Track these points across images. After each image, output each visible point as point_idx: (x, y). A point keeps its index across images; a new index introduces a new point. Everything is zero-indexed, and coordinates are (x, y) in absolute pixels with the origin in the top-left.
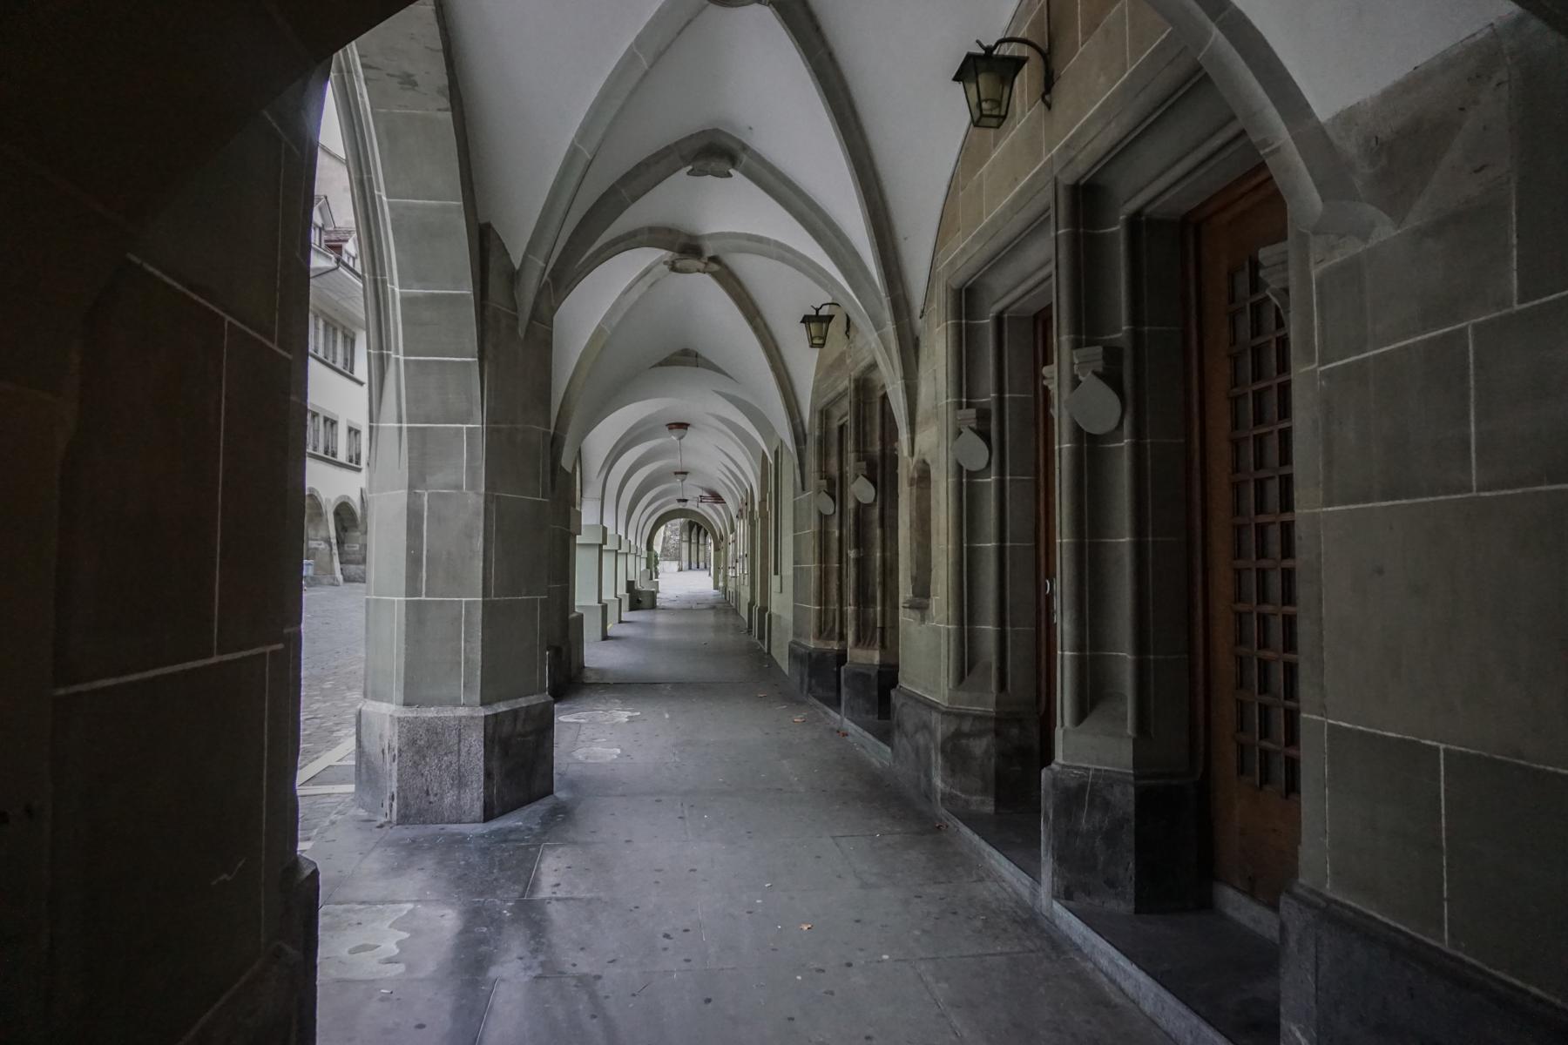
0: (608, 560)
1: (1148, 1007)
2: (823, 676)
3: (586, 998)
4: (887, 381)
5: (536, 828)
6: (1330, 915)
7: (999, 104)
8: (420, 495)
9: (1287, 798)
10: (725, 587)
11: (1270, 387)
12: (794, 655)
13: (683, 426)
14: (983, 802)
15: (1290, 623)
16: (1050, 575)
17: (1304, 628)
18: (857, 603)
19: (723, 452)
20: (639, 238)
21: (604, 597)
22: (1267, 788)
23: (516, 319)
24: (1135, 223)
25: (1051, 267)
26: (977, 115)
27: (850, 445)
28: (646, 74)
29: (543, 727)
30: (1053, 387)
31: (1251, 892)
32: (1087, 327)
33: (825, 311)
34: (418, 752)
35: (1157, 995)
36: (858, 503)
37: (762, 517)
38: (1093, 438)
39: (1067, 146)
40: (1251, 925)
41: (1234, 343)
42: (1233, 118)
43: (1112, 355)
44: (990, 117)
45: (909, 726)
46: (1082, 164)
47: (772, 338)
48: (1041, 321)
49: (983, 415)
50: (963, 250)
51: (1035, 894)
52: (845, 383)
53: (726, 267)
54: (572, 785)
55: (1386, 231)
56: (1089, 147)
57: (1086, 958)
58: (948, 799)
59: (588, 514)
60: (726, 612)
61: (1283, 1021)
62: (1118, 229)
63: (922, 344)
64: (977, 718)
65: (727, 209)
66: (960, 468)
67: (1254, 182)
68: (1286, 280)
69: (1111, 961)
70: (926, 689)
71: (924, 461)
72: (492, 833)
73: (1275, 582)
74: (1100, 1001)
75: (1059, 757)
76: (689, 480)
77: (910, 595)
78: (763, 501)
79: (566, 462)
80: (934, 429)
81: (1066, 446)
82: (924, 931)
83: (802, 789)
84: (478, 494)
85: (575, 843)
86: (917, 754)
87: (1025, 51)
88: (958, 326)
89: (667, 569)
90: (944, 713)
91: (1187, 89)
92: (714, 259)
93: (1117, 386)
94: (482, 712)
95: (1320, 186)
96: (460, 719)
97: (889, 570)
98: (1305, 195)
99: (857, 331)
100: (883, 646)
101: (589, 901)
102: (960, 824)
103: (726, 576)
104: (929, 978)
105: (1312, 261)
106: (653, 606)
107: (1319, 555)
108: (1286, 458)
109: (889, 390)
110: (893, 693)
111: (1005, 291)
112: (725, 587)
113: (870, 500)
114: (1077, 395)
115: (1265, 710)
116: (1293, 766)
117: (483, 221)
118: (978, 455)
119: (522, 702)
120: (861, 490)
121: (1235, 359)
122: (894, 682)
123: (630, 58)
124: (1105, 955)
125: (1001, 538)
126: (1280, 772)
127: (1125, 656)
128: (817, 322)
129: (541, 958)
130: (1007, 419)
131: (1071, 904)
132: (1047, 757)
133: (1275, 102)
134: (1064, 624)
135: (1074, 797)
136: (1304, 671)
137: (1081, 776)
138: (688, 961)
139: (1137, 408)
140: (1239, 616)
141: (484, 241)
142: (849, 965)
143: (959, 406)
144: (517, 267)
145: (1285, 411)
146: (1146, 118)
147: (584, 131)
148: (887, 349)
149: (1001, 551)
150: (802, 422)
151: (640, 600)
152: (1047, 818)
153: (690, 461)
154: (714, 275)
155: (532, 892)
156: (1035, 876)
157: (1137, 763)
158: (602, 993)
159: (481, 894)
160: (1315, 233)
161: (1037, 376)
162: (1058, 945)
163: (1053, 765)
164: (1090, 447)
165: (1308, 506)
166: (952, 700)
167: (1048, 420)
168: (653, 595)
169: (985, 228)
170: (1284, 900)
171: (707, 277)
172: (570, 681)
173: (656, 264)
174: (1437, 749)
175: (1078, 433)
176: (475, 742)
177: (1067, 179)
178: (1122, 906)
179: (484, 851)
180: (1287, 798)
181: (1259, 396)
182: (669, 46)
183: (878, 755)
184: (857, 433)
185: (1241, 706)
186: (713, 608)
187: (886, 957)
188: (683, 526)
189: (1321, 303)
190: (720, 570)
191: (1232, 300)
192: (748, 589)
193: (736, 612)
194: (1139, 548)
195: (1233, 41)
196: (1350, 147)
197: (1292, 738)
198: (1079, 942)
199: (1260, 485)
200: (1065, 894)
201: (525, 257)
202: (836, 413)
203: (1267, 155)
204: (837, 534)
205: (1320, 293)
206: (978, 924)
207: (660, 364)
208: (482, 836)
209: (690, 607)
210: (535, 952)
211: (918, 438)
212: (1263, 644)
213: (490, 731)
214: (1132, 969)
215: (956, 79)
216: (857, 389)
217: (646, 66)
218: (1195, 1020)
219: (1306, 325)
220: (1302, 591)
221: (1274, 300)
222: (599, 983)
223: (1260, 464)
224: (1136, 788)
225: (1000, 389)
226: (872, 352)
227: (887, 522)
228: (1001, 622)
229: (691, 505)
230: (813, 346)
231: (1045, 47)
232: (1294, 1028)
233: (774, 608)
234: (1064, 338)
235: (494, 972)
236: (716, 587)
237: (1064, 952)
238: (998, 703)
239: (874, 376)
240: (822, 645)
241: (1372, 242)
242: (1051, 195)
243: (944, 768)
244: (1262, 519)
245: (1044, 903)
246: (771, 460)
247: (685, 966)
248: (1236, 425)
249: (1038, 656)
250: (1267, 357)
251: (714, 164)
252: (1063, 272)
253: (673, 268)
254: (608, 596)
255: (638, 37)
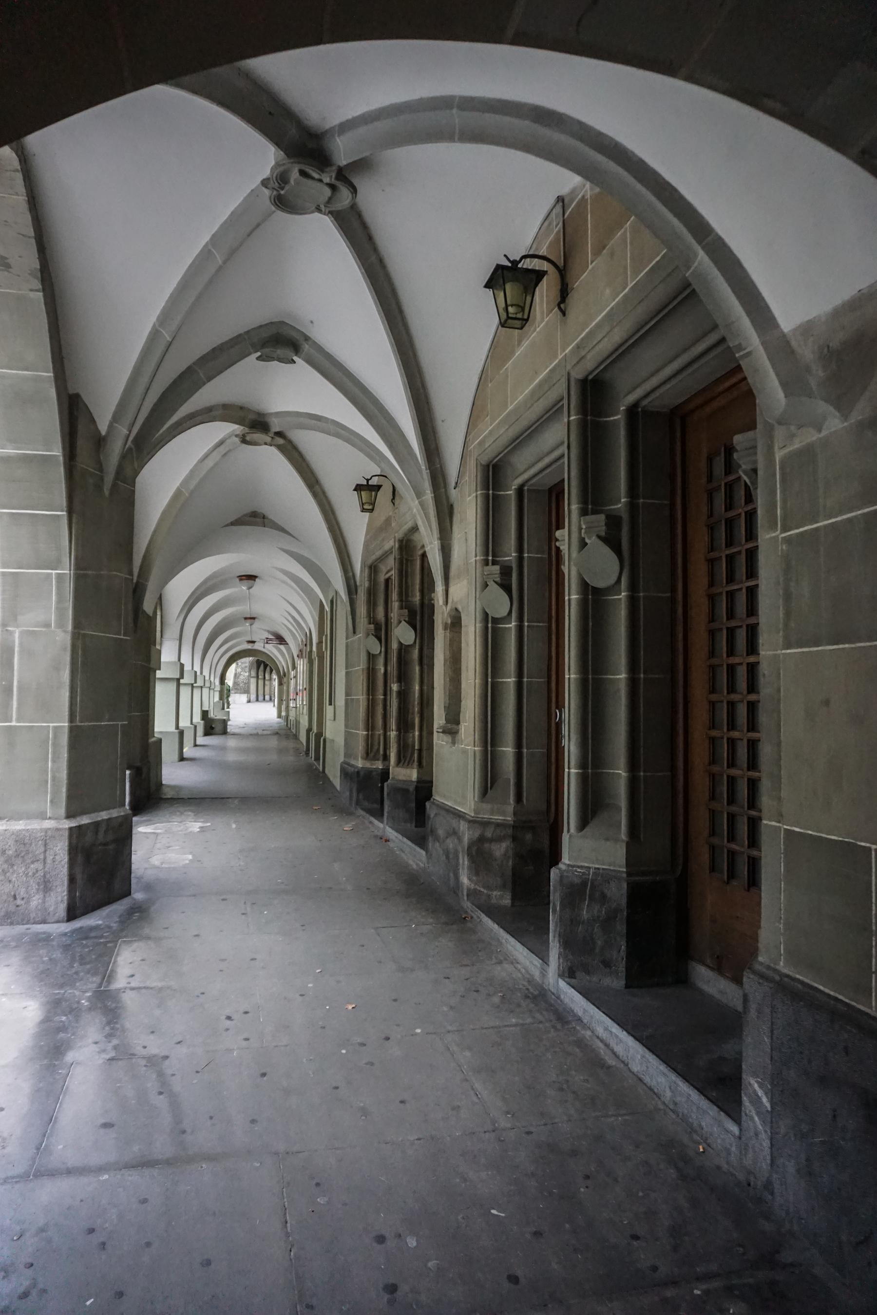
0: (185, 692)
1: (636, 1068)
2: (368, 790)
3: (154, 1076)
4: (426, 541)
5: (115, 926)
6: (784, 988)
7: (523, 309)
8: (11, 633)
9: (748, 890)
10: (287, 717)
11: (739, 552)
12: (346, 774)
13: (252, 578)
14: (502, 897)
15: (753, 745)
16: (560, 705)
17: (766, 751)
18: (399, 729)
19: (285, 601)
20: (214, 413)
21: (181, 724)
22: (734, 883)
23: (102, 479)
24: (632, 412)
25: (564, 449)
26: (504, 316)
27: (395, 596)
28: (220, 268)
29: (121, 837)
30: (564, 548)
31: (719, 968)
32: (593, 498)
33: (374, 481)
34: (6, 861)
35: (643, 1057)
36: (400, 644)
37: (319, 658)
38: (596, 591)
39: (578, 347)
40: (718, 996)
41: (711, 515)
42: (715, 327)
43: (613, 522)
44: (515, 319)
45: (441, 832)
46: (589, 364)
47: (329, 503)
48: (556, 493)
49: (506, 571)
50: (491, 432)
51: (544, 973)
52: (390, 543)
53: (290, 442)
54: (148, 887)
55: (835, 424)
56: (597, 348)
57: (586, 1027)
58: (472, 894)
59: (167, 654)
60: (287, 737)
61: (744, 1076)
62: (618, 417)
63: (455, 511)
64: (498, 825)
65: (291, 391)
66: (486, 615)
67: (727, 384)
68: (755, 462)
69: (606, 1029)
70: (455, 802)
71: (456, 609)
72: (74, 931)
73: (742, 711)
74: (594, 1062)
75: (566, 859)
76: (257, 625)
77: (443, 722)
78: (320, 643)
79: (148, 606)
80: (465, 582)
81: (574, 597)
82: (451, 1007)
83: (349, 888)
84: (65, 632)
85: (149, 938)
86: (447, 857)
87: (545, 266)
88: (486, 497)
89: (238, 700)
90: (470, 822)
91: (677, 301)
92: (279, 434)
93: (616, 548)
94: (67, 824)
95: (784, 385)
96: (46, 830)
97: (426, 702)
98: (772, 392)
99: (401, 497)
100: (420, 765)
101: (161, 989)
102: (483, 916)
103: (287, 707)
104: (455, 1048)
105: (776, 448)
106: (224, 732)
107: (779, 690)
108: (752, 610)
109: (427, 549)
110: (428, 804)
111: (525, 468)
112: (287, 717)
113: (411, 642)
114: (584, 555)
115: (732, 818)
116: (754, 865)
117: (71, 392)
118: (501, 604)
119: (104, 815)
120: (403, 634)
121: (711, 528)
122: (429, 796)
123: (206, 254)
124: (601, 1026)
125: (520, 674)
126: (743, 870)
127: (620, 772)
128: (367, 490)
129: (115, 1042)
130: (527, 577)
131: (573, 980)
132: (555, 858)
133: (749, 313)
134: (571, 747)
135: (579, 890)
136: (765, 785)
137: (584, 874)
138: (247, 1039)
139: (632, 565)
140: (713, 740)
141: (73, 410)
142: (387, 1039)
143: (486, 562)
144: (103, 433)
145: (752, 572)
146: (642, 327)
147: (164, 317)
148: (426, 515)
149: (519, 685)
150: (354, 576)
151: (213, 727)
152: (554, 911)
153: (257, 608)
154: (280, 448)
155: (109, 982)
156: (544, 958)
157: (630, 862)
158: (169, 1072)
159: (61, 986)
160: (780, 423)
161: (551, 539)
162: (562, 1017)
163: (561, 865)
164: (594, 598)
165: (770, 648)
166: (476, 811)
167: (560, 574)
168: (224, 722)
169: (508, 415)
170: (748, 979)
171: (273, 449)
172: (150, 797)
173: (229, 436)
174: (870, 849)
175: (585, 587)
176: (60, 851)
177: (578, 374)
178: (617, 982)
179: (66, 948)
180: (748, 890)
181: (731, 559)
182: (241, 245)
183: (414, 857)
184: (400, 586)
185: (713, 815)
186: (277, 733)
187: (418, 1031)
188: (251, 664)
189: (783, 480)
190: (283, 701)
191: (710, 479)
192: (306, 718)
193: (296, 737)
194: (633, 683)
195: (716, 262)
196: (807, 353)
197: (754, 841)
198: (580, 1014)
199: (731, 632)
200: (569, 973)
201: (111, 426)
202: (383, 568)
203: (743, 357)
204: (382, 671)
205: (783, 475)
206: (496, 1000)
207: (234, 523)
208: (65, 934)
209: (258, 734)
210: (109, 1036)
211: (452, 590)
212: (732, 764)
213: (74, 841)
214: (623, 1035)
215: (488, 285)
216: (401, 548)
217: (220, 262)
218: (673, 1077)
219: (771, 499)
220: (764, 718)
221: (745, 478)
222: (167, 1062)
223: (731, 615)
224: (628, 884)
225: (520, 550)
226: (414, 516)
227: (425, 661)
228: (519, 745)
229: (258, 646)
230: (364, 510)
231: (561, 263)
232: (752, 1081)
233: (328, 734)
234: (575, 507)
235: (70, 1057)
236: (279, 716)
237: (568, 1023)
238: (515, 814)
239: (415, 537)
240: (368, 765)
241: (824, 433)
242: (565, 385)
243: (470, 868)
244: (732, 660)
245: (551, 981)
246: (327, 608)
247: (245, 1043)
248: (712, 584)
249: (549, 768)
250: (739, 527)
251: (280, 352)
252: (573, 437)
253: (244, 441)
254: (184, 723)
255: (214, 235)
